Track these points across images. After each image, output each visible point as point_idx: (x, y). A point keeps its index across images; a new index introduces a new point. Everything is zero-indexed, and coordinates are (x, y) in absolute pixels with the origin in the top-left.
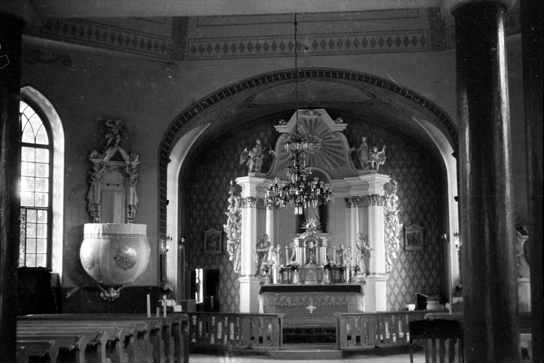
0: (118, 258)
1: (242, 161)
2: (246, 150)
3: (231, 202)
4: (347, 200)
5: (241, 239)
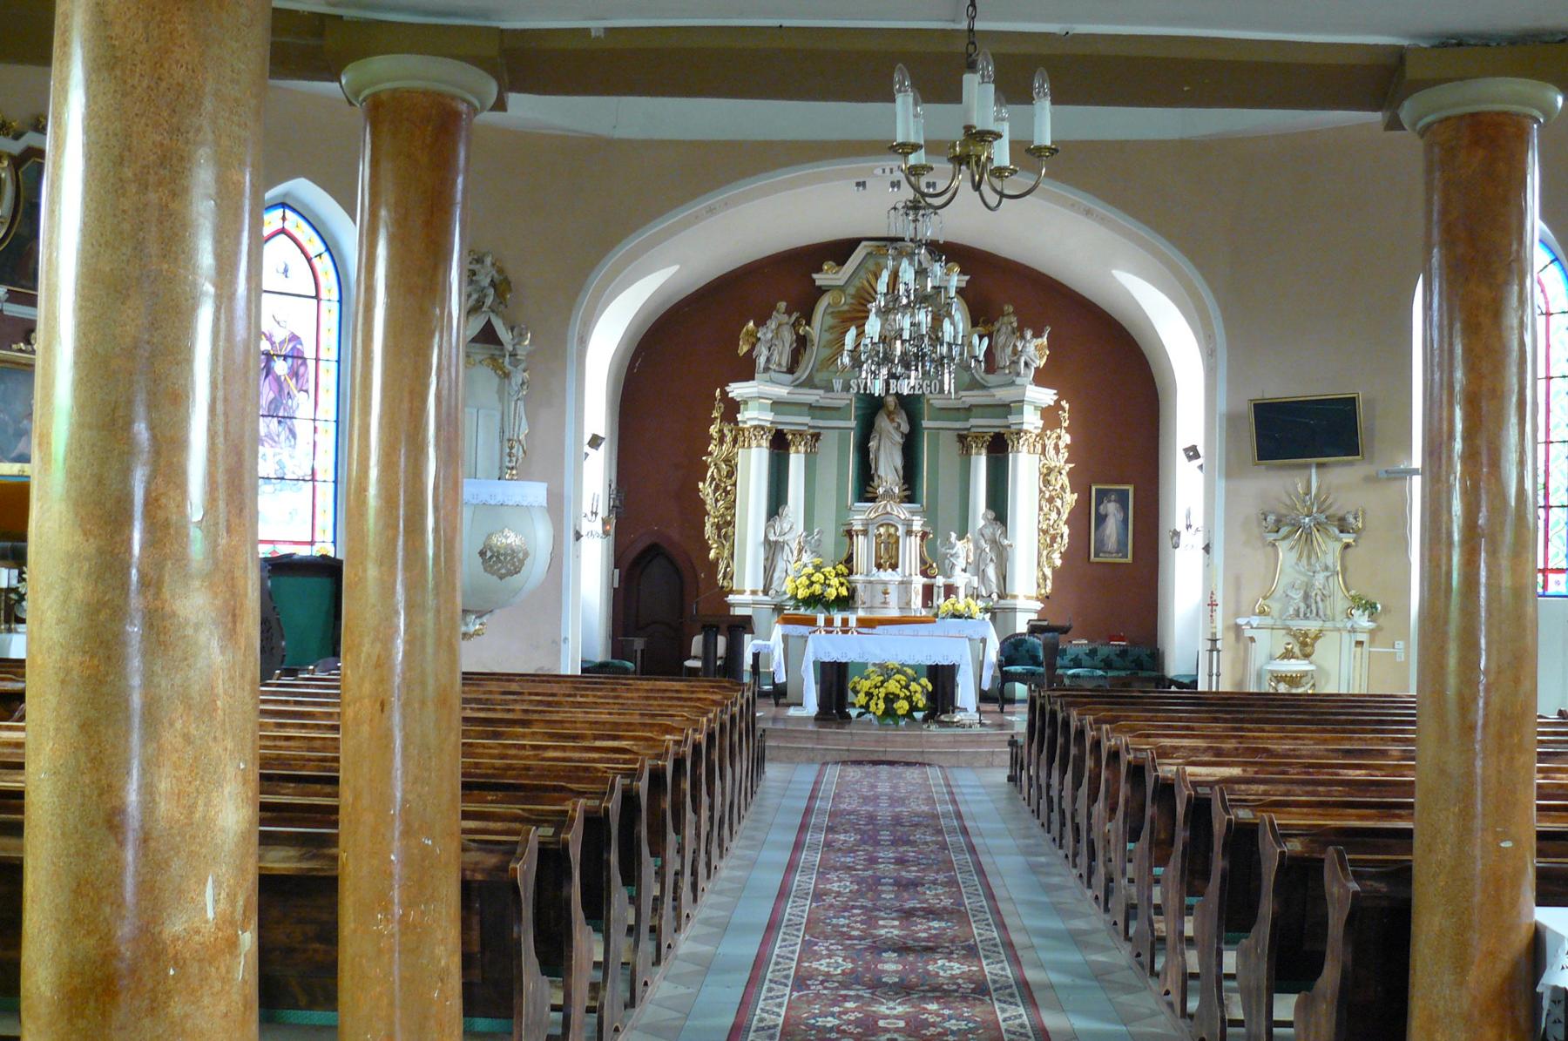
0: (489, 554)
1: (743, 349)
2: (751, 324)
3: (715, 435)
4: (962, 438)
5: (734, 514)
